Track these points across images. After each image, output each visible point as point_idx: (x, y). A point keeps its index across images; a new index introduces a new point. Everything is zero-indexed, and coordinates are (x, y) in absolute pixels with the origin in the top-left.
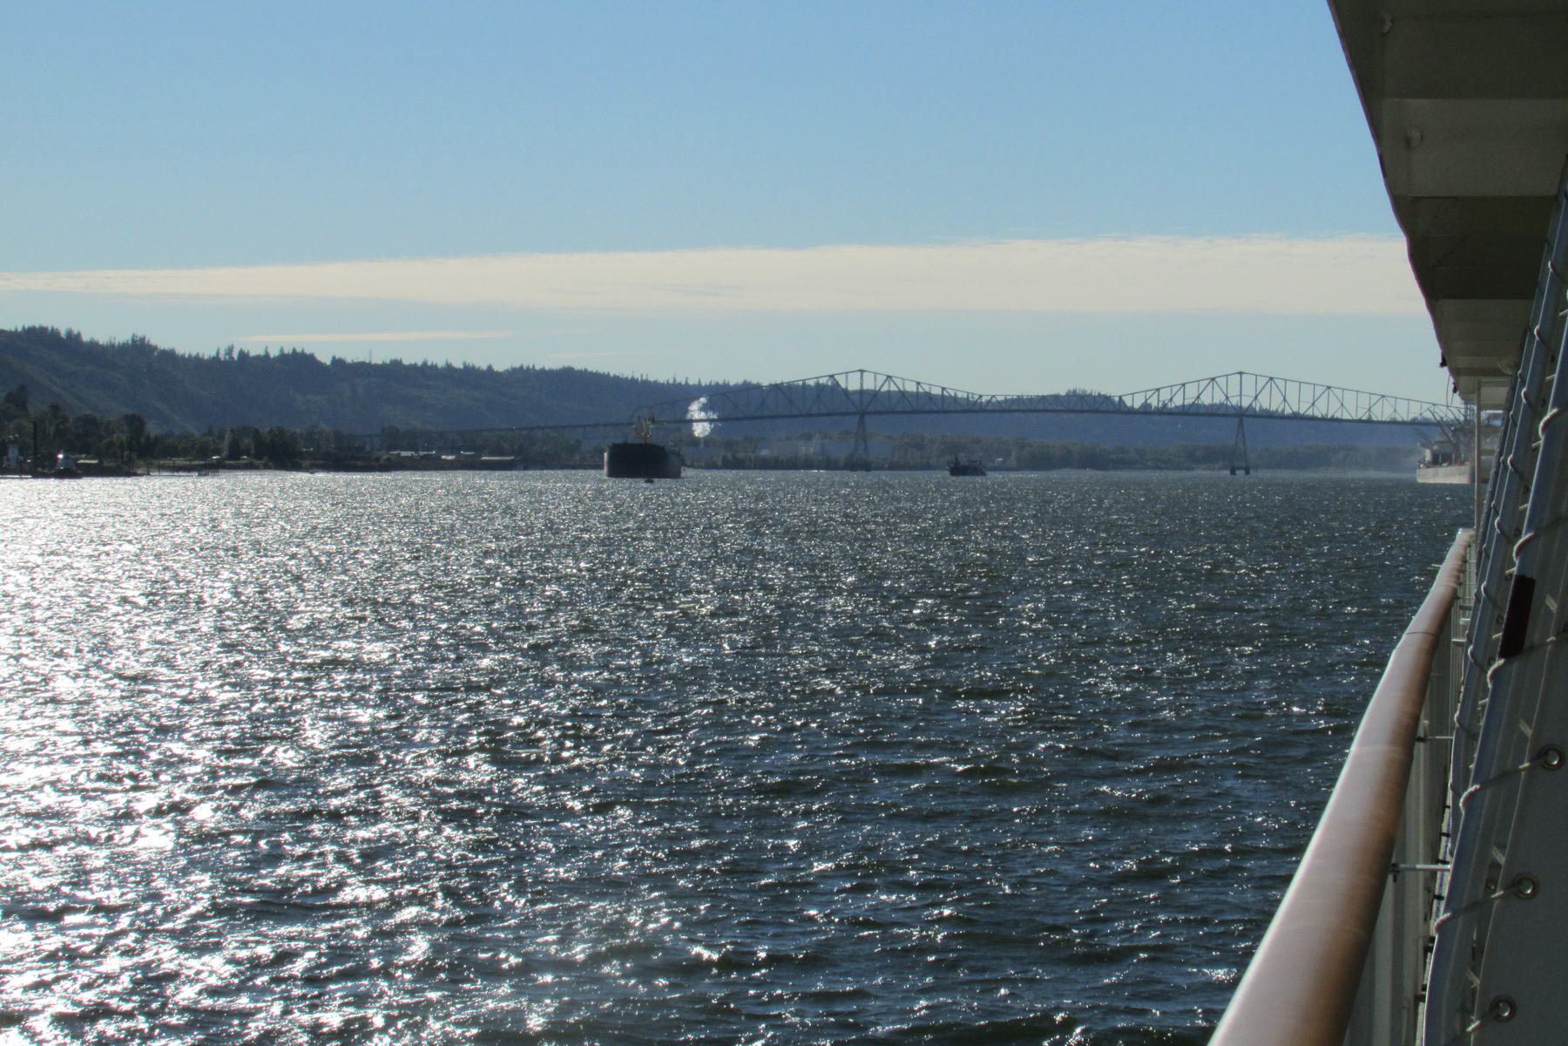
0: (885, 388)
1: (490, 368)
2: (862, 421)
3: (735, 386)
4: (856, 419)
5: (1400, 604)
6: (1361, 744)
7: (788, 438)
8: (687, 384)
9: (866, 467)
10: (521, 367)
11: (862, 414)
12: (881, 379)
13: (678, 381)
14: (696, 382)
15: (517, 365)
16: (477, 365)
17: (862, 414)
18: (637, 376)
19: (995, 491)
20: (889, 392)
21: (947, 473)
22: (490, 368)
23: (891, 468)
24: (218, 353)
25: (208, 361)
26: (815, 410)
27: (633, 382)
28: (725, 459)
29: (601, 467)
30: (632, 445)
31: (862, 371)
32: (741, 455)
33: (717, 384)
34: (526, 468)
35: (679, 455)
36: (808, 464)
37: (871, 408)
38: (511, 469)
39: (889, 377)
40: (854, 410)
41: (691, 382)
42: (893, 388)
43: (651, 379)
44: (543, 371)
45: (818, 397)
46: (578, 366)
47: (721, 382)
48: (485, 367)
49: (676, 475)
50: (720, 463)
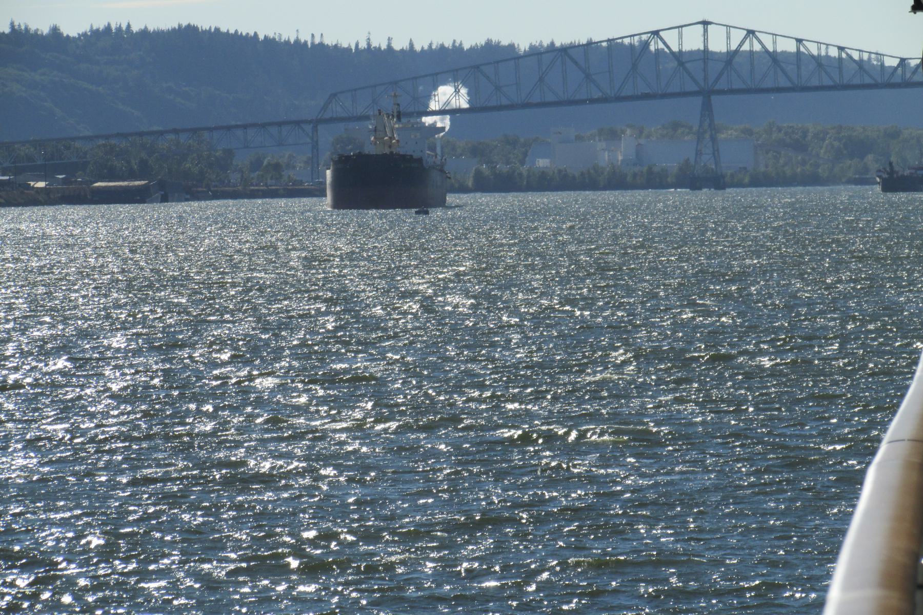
0: (746, 47)
1: (55, 31)
2: (707, 108)
3: (473, 50)
4: (698, 101)
5: (909, 366)
6: (848, 586)
7: (579, 138)
8: (390, 48)
9: (718, 182)
10: (108, 28)
11: (707, 93)
12: (737, 37)
13: (375, 44)
14: (405, 45)
15: (100, 25)
16: (32, 27)
17: (707, 93)
18: (305, 37)
19: (505, 211)
20: (751, 53)
21: (878, 188)
22: (55, 31)
23: (756, 182)
24: (210, 27)
25: (505, 47)
26: (627, 91)
27: (298, 47)
28: (478, 174)
29: (323, 194)
30: (369, 156)
31: (705, 23)
32: (502, 168)
33: (442, 46)
34: (164, 199)
35: (442, 171)
36: (617, 182)
37: (722, 85)
38: (142, 201)
39: (751, 33)
40: (696, 88)
41: (397, 46)
42: (757, 47)
43: (329, 41)
44: (144, 33)
45: (634, 66)
46: (205, 23)
47: (448, 44)
48: (45, 30)
49: (441, 203)
50: (470, 183)
